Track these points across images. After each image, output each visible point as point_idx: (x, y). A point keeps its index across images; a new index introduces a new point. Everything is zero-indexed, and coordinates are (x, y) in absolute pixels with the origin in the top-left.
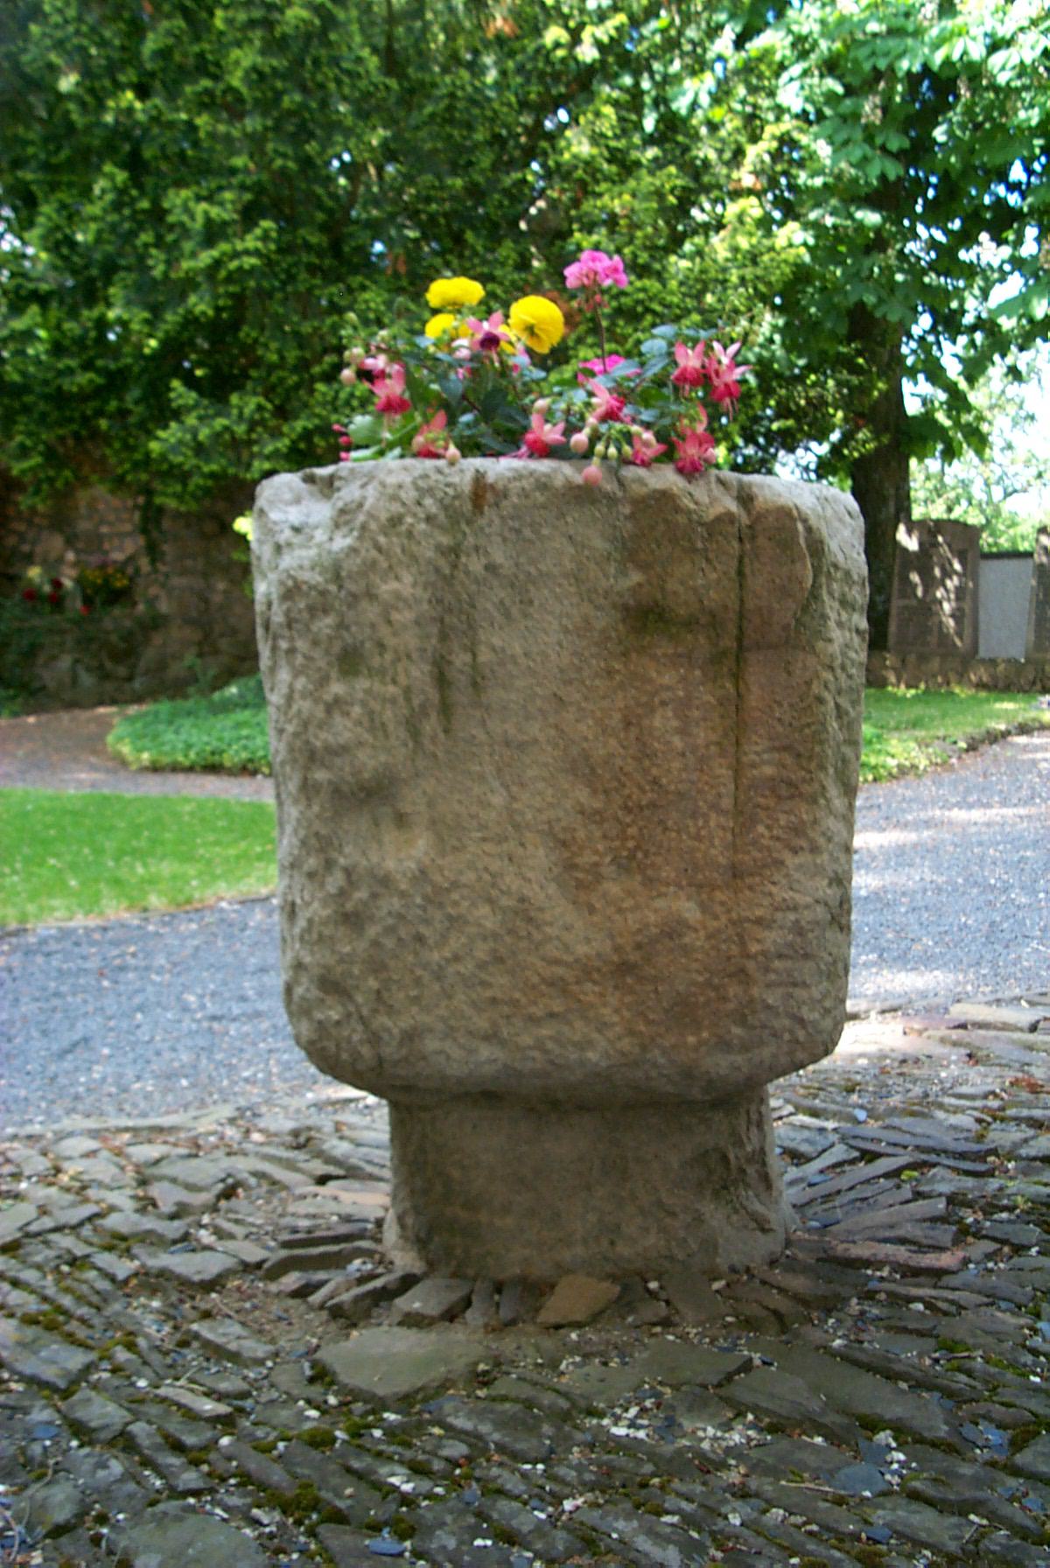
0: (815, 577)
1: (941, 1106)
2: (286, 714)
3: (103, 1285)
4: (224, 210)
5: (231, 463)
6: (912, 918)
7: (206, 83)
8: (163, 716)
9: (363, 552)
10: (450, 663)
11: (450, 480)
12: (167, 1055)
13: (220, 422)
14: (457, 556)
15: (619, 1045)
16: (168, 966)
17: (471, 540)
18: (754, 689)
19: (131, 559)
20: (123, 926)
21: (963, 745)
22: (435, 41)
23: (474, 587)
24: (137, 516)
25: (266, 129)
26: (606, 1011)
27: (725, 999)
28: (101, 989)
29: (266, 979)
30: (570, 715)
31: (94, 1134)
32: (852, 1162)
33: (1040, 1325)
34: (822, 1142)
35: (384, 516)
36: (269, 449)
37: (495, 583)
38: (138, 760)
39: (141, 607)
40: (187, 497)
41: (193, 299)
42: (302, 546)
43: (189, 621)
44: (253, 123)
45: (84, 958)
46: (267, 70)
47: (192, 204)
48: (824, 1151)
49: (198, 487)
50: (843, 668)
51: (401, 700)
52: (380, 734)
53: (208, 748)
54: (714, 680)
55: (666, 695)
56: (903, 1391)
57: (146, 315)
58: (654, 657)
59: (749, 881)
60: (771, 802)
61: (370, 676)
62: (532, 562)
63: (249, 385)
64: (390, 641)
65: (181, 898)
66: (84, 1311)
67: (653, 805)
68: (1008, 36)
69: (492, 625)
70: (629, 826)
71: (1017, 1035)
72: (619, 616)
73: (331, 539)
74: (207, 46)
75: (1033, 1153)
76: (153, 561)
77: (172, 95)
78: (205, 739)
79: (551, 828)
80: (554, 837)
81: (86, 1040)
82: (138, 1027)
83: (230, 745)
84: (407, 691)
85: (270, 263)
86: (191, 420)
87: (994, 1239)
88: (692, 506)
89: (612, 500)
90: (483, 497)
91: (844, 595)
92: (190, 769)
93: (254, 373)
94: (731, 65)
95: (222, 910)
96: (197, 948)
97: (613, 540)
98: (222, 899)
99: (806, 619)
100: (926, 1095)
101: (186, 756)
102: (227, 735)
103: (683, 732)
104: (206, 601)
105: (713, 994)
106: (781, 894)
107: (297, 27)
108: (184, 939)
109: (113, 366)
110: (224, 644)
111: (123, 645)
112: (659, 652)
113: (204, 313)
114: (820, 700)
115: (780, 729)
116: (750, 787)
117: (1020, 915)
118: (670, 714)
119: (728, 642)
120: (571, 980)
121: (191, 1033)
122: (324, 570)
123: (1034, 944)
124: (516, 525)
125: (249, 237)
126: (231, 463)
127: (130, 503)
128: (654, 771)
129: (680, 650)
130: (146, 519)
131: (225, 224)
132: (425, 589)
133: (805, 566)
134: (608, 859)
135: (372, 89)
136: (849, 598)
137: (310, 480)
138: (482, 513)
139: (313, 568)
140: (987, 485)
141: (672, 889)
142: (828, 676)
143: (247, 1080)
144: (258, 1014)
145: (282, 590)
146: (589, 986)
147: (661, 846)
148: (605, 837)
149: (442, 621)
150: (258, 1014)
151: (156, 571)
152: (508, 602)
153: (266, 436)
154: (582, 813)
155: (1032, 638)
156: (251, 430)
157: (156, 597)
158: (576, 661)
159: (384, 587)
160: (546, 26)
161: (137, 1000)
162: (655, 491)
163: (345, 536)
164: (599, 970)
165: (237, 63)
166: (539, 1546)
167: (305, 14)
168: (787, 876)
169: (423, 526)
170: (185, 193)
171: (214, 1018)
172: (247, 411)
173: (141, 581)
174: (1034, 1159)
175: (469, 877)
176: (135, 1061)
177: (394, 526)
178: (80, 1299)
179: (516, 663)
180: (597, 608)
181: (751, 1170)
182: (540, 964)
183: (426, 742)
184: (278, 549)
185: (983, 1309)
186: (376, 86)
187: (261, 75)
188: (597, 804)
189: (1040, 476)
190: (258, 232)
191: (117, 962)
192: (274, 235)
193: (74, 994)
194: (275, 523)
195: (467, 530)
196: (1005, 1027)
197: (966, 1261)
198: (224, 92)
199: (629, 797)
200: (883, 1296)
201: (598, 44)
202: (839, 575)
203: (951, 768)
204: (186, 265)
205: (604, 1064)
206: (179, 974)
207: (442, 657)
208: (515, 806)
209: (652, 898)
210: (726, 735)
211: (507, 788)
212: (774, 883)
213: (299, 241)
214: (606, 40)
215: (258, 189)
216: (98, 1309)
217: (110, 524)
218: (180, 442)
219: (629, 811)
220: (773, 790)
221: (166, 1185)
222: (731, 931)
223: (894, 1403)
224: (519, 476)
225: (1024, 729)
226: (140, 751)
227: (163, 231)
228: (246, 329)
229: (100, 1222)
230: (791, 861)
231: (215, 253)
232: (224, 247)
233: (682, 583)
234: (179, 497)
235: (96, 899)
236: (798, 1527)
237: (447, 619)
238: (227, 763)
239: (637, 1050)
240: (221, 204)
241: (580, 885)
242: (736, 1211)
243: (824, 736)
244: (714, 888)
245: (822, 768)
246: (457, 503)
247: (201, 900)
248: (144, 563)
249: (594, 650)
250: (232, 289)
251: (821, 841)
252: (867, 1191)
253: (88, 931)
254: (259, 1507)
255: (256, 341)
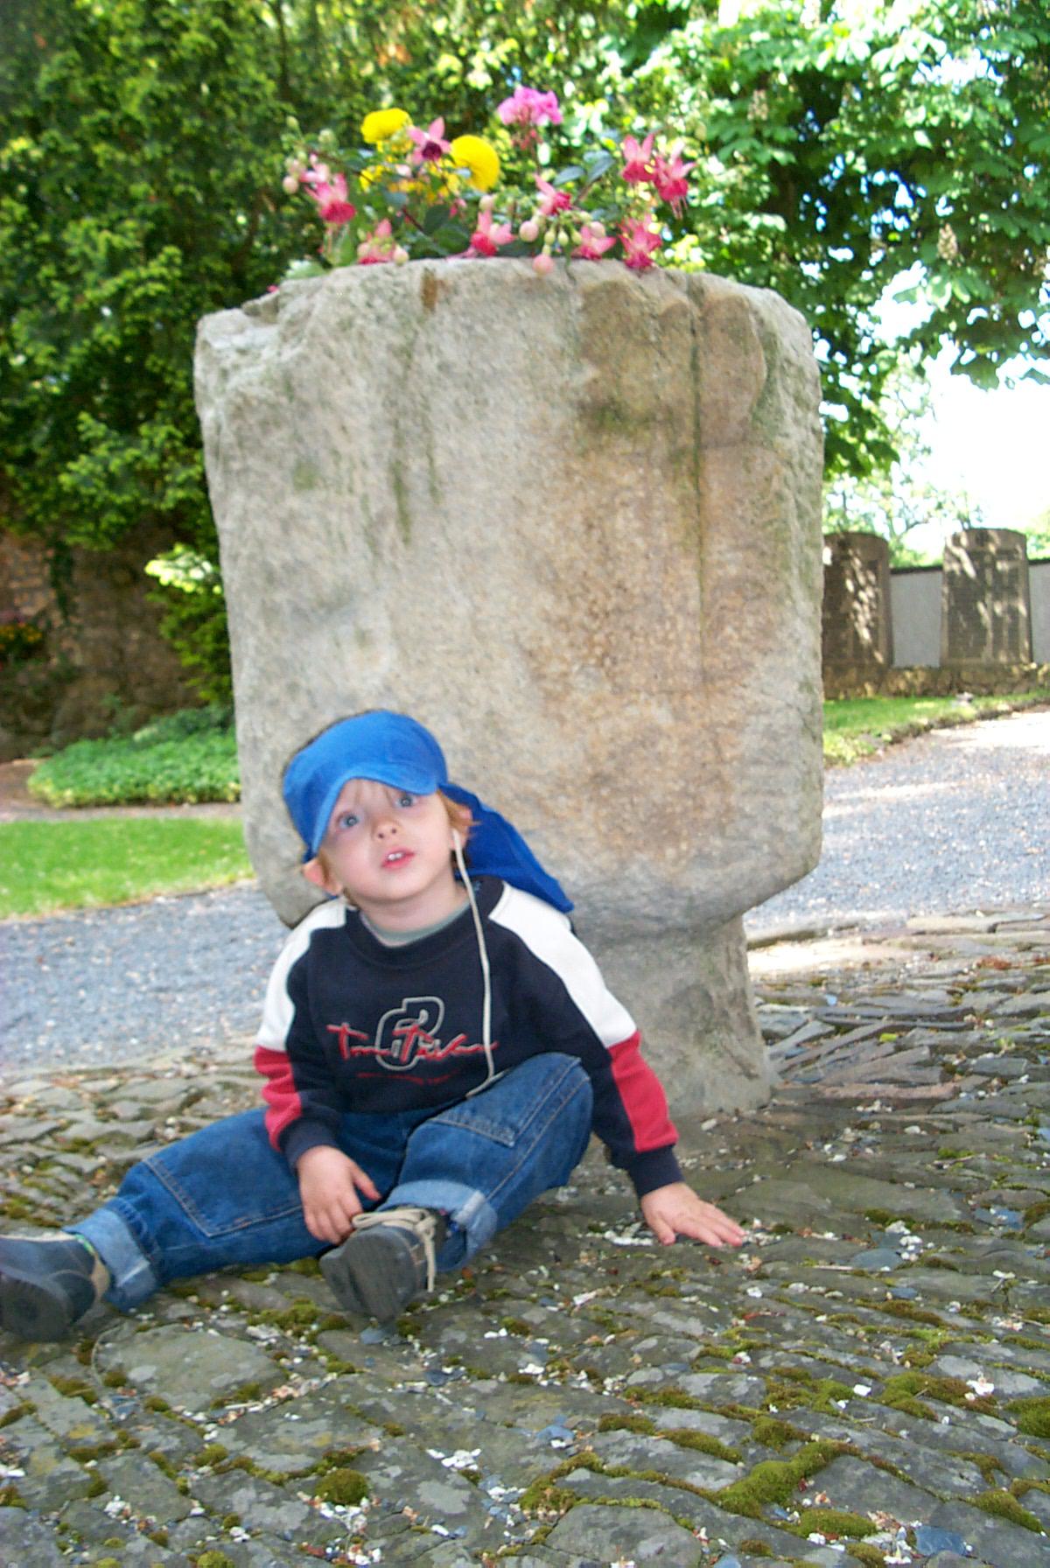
0: (770, 370)
1: (911, 987)
2: (240, 537)
3: (73, 1178)
4: (129, 236)
5: (144, 495)
6: (856, 869)
7: (103, 113)
8: (84, 756)
9: (314, 359)
10: (406, 468)
11: (399, 279)
12: (114, 1023)
13: (131, 453)
14: (410, 356)
15: (596, 861)
16: (109, 951)
17: (423, 339)
18: (715, 485)
19: (43, 613)
20: (58, 921)
21: (888, 737)
22: (329, 70)
23: (427, 388)
24: (47, 570)
25: (165, 155)
26: (580, 826)
27: (701, 807)
28: (41, 973)
29: (210, 955)
30: (529, 521)
31: (43, 1077)
32: (828, 1035)
33: (1039, 1131)
34: (796, 1022)
35: (334, 321)
36: (181, 477)
37: (449, 382)
38: (61, 798)
39: (55, 661)
40: (100, 536)
41: (98, 329)
42: (250, 365)
43: (102, 673)
44: (152, 151)
45: (21, 949)
46: (165, 95)
47: (93, 233)
48: (798, 1029)
49: (111, 524)
50: (802, 467)
51: (358, 509)
52: (338, 545)
53: (132, 781)
54: (675, 480)
55: (627, 496)
56: (910, 1190)
57: (51, 349)
58: (612, 457)
59: (719, 684)
60: (738, 602)
61: (326, 487)
62: (485, 359)
63: (158, 416)
64: (344, 449)
65: (117, 896)
66: (51, 1200)
67: (619, 610)
68: (890, 35)
69: (447, 426)
70: (595, 632)
71: (975, 936)
72: (575, 414)
73: (279, 354)
74: (101, 78)
75: (1009, 1010)
76: (65, 615)
77: (68, 126)
78: (129, 771)
79: (517, 638)
80: (521, 647)
81: (29, 1016)
82: (82, 1001)
83: (154, 776)
84: (365, 499)
85: (176, 293)
86: (101, 451)
87: (983, 1074)
88: (643, 299)
89: (563, 294)
90: (434, 294)
91: (798, 392)
92: (115, 803)
93: (162, 404)
94: (621, 89)
95: (159, 905)
96: (136, 936)
97: (566, 336)
98: (158, 895)
99: (761, 414)
100: (894, 981)
101: (110, 790)
102: (151, 767)
103: (646, 532)
104: (121, 652)
105: (690, 803)
106: (752, 696)
107: (194, 51)
108: (123, 928)
109: (19, 404)
110: (141, 693)
111: (39, 700)
112: (617, 451)
113: (110, 343)
114: (780, 497)
115: (742, 527)
116: (715, 588)
117: (963, 859)
118: (631, 515)
119: (686, 440)
120: (546, 795)
121: (136, 1003)
122: (274, 383)
123: (980, 881)
124: (468, 321)
125: (153, 264)
126: (144, 495)
127: (39, 557)
128: (619, 575)
129: (640, 448)
130: (56, 573)
131: (128, 252)
132: (378, 392)
133: (758, 358)
134: (576, 668)
135: (269, 114)
136: (803, 394)
137: (254, 313)
138: (433, 310)
139: (262, 383)
140: (889, 518)
141: (643, 696)
142: (786, 471)
143: (199, 1034)
144: (204, 985)
145: (232, 408)
146: (562, 799)
147: (628, 652)
148: (572, 645)
149: (396, 424)
150: (204, 985)
151: (68, 624)
152: (462, 402)
153: (178, 465)
154: (548, 620)
155: (946, 643)
156: (163, 458)
157: (71, 650)
158: (534, 462)
159: (337, 393)
160: (437, 56)
161: (81, 979)
162: (605, 284)
163: (294, 347)
164: (572, 782)
165: (133, 91)
166: (553, 1332)
167: (202, 38)
168: (758, 678)
169: (374, 327)
170: (88, 222)
171: (160, 990)
172: (157, 441)
173: (54, 635)
174: (1012, 1015)
175: (434, 690)
176: (81, 1030)
177: (344, 330)
178: (46, 1192)
179: (474, 467)
180: (553, 405)
181: (733, 1014)
182: (511, 779)
183: (386, 552)
184: (225, 374)
185: (980, 1125)
186: (273, 111)
187: (159, 102)
188: (563, 610)
189: (940, 506)
190: (162, 258)
191: (56, 950)
192: (178, 261)
193: (14, 979)
194: (219, 351)
195: (419, 329)
196: (964, 931)
197: (957, 1092)
198: (121, 122)
199: (594, 602)
200: (876, 1125)
201: (490, 70)
202: (792, 371)
203: (879, 759)
204: (90, 294)
205: (582, 883)
206: (120, 956)
207: (399, 462)
208: (479, 616)
209: (624, 706)
210: (688, 534)
211: (470, 597)
212: (745, 686)
213: (202, 270)
214: (497, 65)
215: (158, 217)
216: (66, 1198)
217: (20, 579)
218: (92, 474)
219: (595, 616)
220: (739, 590)
221: (126, 1104)
222: (705, 736)
223: (902, 1199)
224: (469, 273)
225: (945, 723)
226: (62, 789)
227: (64, 264)
228: (186, 123)
229: (59, 1134)
230: (761, 663)
231: (119, 281)
232: (129, 274)
233: (637, 378)
234: (92, 535)
235: (30, 901)
236: (822, 1294)
237: (402, 422)
238: (153, 795)
239: (615, 866)
240: (123, 234)
241: (550, 696)
242: (721, 1056)
243: (786, 535)
244: (684, 694)
245: (787, 568)
246: (407, 301)
247: (137, 896)
248: (56, 617)
249: (552, 450)
250: (139, 317)
251: (789, 643)
252: (848, 1052)
253: (23, 928)
254: (254, 1324)
255: (163, 369)
